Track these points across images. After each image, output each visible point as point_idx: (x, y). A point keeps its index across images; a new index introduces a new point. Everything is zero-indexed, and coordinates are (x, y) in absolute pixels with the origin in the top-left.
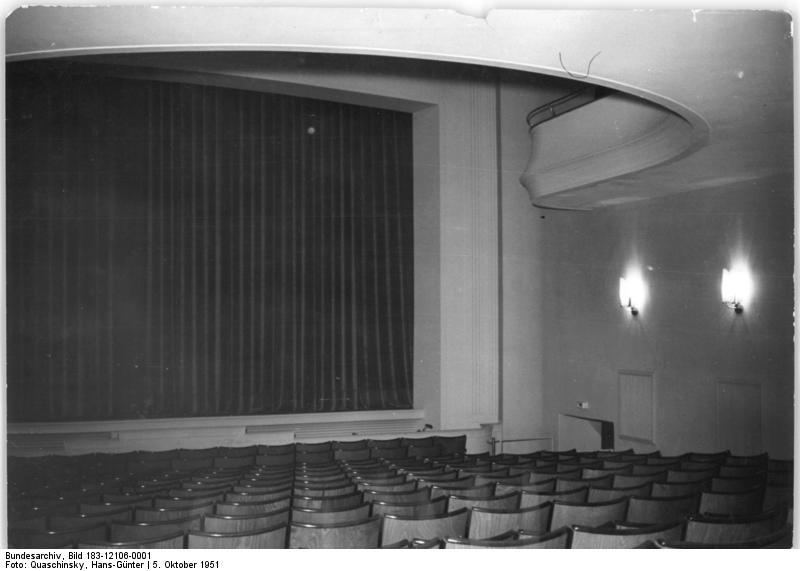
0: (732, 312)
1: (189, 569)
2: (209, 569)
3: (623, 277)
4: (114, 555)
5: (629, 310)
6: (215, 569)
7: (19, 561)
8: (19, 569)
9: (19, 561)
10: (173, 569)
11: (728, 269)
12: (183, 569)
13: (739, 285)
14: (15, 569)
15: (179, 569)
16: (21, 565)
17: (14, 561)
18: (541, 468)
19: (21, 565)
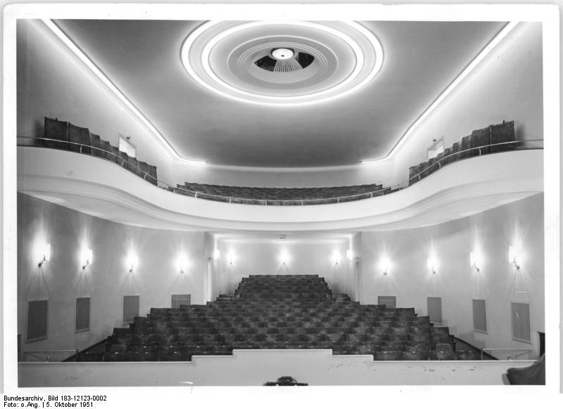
0: (432, 273)
1: (72, 407)
2: (86, 407)
3: (471, 251)
4: (81, 398)
5: (431, 270)
6: (90, 407)
7: (14, 402)
8: (14, 408)
9: (14, 402)
10: (60, 408)
11: (317, 276)
12: (68, 408)
13: (517, 254)
14: (11, 407)
15: (65, 408)
16: (15, 405)
17: (10, 402)
18: (515, 315)
19: (15, 405)
